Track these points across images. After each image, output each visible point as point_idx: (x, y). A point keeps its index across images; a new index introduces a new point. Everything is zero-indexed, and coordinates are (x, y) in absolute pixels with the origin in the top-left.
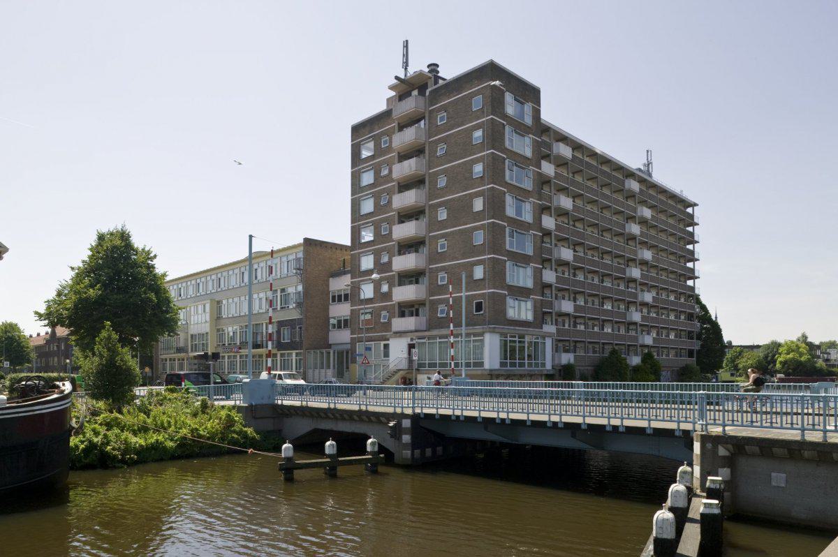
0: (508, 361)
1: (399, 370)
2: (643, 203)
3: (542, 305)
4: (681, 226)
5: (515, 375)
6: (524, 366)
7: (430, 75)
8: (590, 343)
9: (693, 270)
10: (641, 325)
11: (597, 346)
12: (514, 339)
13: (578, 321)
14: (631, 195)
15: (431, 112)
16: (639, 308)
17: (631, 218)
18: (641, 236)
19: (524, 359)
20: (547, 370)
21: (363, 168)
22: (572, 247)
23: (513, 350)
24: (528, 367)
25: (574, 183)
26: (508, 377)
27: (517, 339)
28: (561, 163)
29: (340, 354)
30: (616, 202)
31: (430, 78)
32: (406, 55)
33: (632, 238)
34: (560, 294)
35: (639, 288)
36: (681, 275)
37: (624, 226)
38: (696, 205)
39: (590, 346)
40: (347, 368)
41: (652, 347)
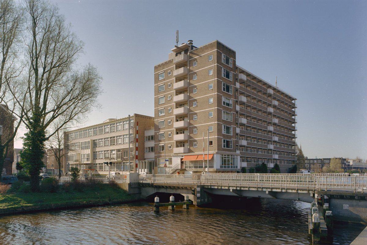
0: (223, 165)
1: (178, 169)
2: (274, 98)
3: (236, 142)
4: (290, 108)
5: (225, 171)
6: (229, 168)
7: (189, 45)
8: (253, 158)
9: (294, 127)
10: (274, 150)
11: (256, 159)
12: (225, 156)
13: (259, 150)
14: (270, 95)
15: (190, 61)
16: (273, 143)
17: (270, 105)
18: (274, 113)
19: (229, 165)
20: (238, 169)
21: (160, 84)
22: (246, 118)
23: (225, 161)
24: (231, 168)
25: (247, 91)
26: (223, 172)
27: (227, 156)
28: (242, 82)
29: (150, 163)
30: (253, 93)
31: (190, 46)
32: (177, 37)
33: (270, 113)
34: (241, 138)
35: (273, 134)
36: (290, 129)
37: (267, 109)
38: (296, 99)
39: (253, 159)
40: (153, 168)
41: (278, 159)
